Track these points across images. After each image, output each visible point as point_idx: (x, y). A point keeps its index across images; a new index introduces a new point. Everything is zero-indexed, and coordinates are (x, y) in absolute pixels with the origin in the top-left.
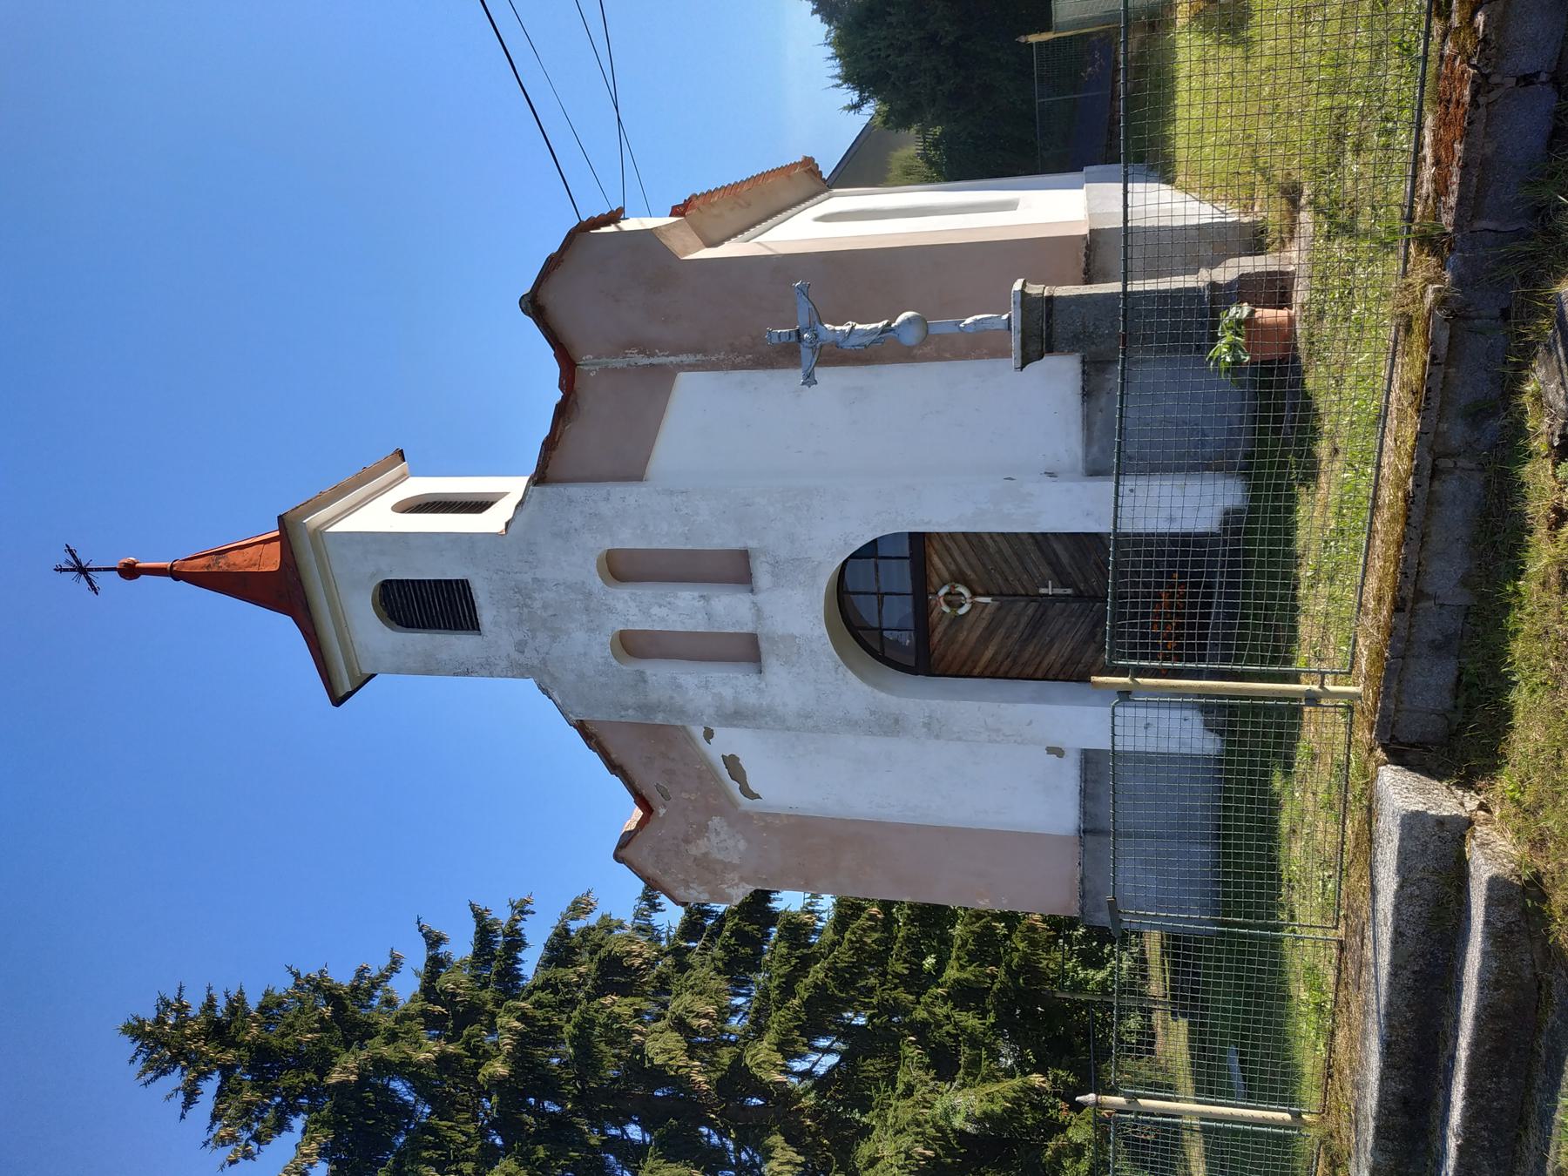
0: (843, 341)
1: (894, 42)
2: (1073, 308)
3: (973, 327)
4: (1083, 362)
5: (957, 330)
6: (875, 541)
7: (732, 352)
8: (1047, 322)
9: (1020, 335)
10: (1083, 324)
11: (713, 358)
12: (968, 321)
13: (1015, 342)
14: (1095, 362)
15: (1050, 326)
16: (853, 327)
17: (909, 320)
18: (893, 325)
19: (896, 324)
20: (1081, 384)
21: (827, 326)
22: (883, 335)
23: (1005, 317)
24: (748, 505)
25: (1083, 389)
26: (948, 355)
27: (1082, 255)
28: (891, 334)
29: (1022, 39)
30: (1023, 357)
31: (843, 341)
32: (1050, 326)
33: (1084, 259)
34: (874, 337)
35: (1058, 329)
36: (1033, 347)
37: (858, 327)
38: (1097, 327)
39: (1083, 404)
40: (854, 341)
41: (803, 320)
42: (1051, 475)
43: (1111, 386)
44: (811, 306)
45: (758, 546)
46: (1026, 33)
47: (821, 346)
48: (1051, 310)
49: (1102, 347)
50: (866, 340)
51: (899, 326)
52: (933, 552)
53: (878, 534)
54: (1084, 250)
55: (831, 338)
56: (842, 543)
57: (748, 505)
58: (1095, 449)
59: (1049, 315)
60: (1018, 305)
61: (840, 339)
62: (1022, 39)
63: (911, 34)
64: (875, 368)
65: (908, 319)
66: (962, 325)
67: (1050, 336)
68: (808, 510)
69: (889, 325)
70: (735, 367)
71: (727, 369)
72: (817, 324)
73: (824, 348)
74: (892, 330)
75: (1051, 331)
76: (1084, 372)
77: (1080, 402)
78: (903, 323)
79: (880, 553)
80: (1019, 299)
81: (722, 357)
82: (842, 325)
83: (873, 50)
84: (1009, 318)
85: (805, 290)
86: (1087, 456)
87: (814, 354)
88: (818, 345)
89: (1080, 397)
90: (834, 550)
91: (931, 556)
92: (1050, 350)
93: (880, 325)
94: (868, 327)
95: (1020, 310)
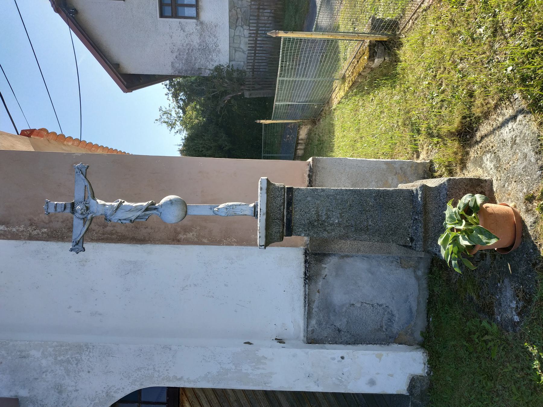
0: (112, 215)
1: (205, 145)
2: (309, 199)
3: (225, 210)
4: (306, 254)
5: (212, 213)
6: (141, 389)
7: (31, 225)
8: (288, 209)
9: (265, 217)
10: (317, 212)
11: (14, 230)
12: (221, 206)
13: (260, 222)
14: (316, 254)
15: (289, 212)
16: (121, 203)
17: (171, 202)
18: (157, 205)
19: (160, 204)
20: (303, 270)
21: (98, 201)
22: (147, 213)
23: (252, 205)
24: (24, 357)
25: (305, 274)
26: (205, 241)
27: (306, 176)
28: (155, 211)
29: (258, 121)
30: (266, 237)
31: (112, 215)
32: (289, 212)
33: (307, 179)
34: (139, 213)
35: (296, 216)
36: (276, 229)
37: (126, 203)
38: (328, 217)
39: (305, 286)
40: (120, 215)
41: (79, 195)
42: (280, 341)
43: (325, 273)
44: (87, 183)
45: (28, 395)
46: (260, 119)
47: (92, 219)
48: (292, 199)
49: (333, 233)
50: (133, 216)
51: (162, 206)
52: (185, 399)
53: (137, 388)
54: (308, 173)
55: (101, 211)
56: (104, 394)
57: (24, 357)
58: (313, 322)
59: (290, 203)
60: (264, 191)
61: (109, 213)
62: (258, 121)
63: (212, 144)
64: (148, 247)
65: (171, 200)
66: (215, 209)
67: (289, 221)
68: (77, 364)
69: (153, 204)
70: (31, 238)
71: (25, 239)
72: (90, 198)
73: (94, 220)
74: (156, 209)
75: (291, 216)
76: (306, 261)
77: (303, 284)
78: (166, 203)
79: (143, 399)
80: (265, 186)
81: (21, 229)
82: (113, 202)
83: (197, 148)
84: (255, 207)
85: (84, 170)
86: (307, 327)
87: (84, 223)
88: (89, 217)
89: (303, 280)
90: (97, 401)
91: (183, 402)
92: (289, 234)
93: (145, 204)
94: (134, 205)
95: (266, 195)
